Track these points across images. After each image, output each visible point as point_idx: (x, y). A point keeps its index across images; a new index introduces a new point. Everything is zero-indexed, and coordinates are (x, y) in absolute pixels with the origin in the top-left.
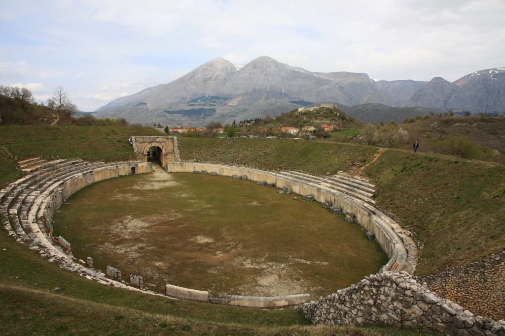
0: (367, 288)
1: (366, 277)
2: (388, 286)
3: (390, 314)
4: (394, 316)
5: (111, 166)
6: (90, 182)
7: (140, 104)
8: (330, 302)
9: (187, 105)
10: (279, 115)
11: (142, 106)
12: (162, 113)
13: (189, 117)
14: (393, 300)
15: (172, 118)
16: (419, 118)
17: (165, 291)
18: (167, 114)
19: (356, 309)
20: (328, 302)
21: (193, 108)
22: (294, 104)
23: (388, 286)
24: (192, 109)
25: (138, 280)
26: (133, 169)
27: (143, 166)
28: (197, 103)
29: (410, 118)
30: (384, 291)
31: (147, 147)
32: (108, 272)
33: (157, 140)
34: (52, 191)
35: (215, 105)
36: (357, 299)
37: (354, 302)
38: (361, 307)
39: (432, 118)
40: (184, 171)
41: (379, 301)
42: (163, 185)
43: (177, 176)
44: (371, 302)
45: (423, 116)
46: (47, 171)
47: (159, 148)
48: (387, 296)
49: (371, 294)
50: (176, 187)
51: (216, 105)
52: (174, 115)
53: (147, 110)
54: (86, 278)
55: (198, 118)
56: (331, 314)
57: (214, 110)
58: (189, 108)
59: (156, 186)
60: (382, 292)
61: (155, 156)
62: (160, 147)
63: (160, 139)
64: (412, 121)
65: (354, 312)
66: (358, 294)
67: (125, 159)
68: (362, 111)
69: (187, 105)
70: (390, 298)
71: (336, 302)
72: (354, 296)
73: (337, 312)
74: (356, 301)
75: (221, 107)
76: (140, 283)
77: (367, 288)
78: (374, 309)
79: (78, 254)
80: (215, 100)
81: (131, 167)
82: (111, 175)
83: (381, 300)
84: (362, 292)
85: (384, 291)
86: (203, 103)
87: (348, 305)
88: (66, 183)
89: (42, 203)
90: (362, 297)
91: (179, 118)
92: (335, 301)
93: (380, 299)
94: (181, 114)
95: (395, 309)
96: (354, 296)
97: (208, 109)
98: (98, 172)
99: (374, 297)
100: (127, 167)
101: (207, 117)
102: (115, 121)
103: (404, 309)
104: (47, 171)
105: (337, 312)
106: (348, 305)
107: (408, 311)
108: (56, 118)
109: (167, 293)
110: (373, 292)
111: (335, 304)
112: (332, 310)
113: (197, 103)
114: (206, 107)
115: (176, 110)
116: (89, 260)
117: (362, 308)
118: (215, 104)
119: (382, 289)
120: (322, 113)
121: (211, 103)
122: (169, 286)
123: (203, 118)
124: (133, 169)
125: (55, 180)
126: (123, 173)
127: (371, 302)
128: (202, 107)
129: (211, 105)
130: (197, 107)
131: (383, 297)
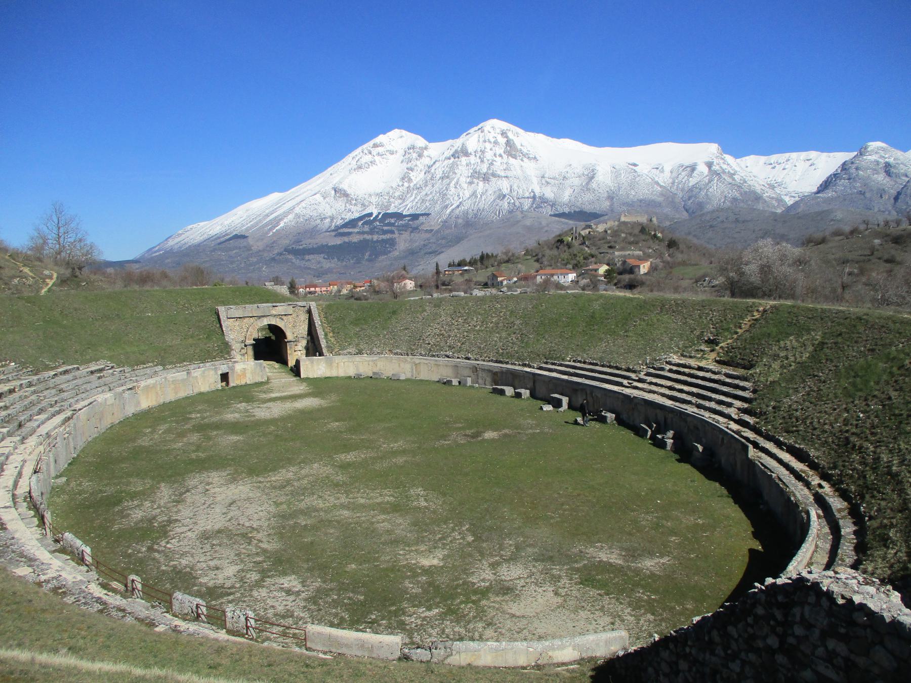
0: (760, 611)
1: (756, 584)
2: (809, 604)
3: (821, 669)
4: (831, 674)
5: (176, 375)
6: (130, 410)
7: (230, 239)
8: (676, 646)
9: (333, 234)
10: (531, 243)
11: (242, 243)
12: (281, 254)
13: (339, 260)
14: (824, 635)
15: (303, 263)
16: (837, 233)
17: (302, 641)
18: (290, 257)
19: (738, 662)
20: (671, 646)
21: (346, 239)
22: (563, 220)
23: (809, 604)
24: (345, 242)
25: (243, 619)
26: (225, 377)
27: (247, 369)
28: (356, 230)
29: (818, 235)
30: (802, 614)
31: (255, 330)
32: (176, 607)
33: (274, 312)
34: (48, 435)
35: (392, 232)
36: (740, 636)
37: (734, 646)
38: (750, 654)
39: (867, 232)
40: (334, 373)
41: (791, 640)
42: (289, 406)
43: (319, 386)
44: (773, 641)
45: (847, 229)
46: (34, 392)
47: (273, 329)
48: (809, 626)
49: (772, 623)
50: (320, 410)
51: (396, 232)
52: (307, 257)
53: (248, 248)
54: (484, 440)
55: (358, 262)
56: (681, 674)
57: (392, 243)
58: (338, 241)
59: (276, 410)
60: (798, 619)
61: (270, 347)
62: (280, 324)
63: (281, 308)
64: (823, 241)
65: (735, 666)
66: (740, 626)
67: (205, 357)
68: (711, 226)
69: (333, 234)
70: (817, 632)
71: (691, 647)
72: (731, 630)
73: (694, 669)
74: (736, 640)
75: (406, 235)
76: (248, 627)
77: (760, 611)
78: (780, 658)
79: (109, 570)
80: (393, 221)
81: (220, 372)
82: (176, 393)
83: (797, 637)
84: (750, 620)
85: (802, 614)
86: (366, 228)
87: (719, 651)
88: (78, 418)
89: (24, 461)
90: (750, 630)
91: (319, 263)
92: (689, 643)
93: (793, 635)
94: (322, 255)
95: (830, 657)
96: (731, 630)
97: (377, 241)
98: (147, 388)
99: (779, 630)
100: (212, 372)
101: (376, 257)
102: (709, 207)
103: (852, 657)
104: (34, 392)
105: (694, 669)
106: (719, 651)
107: (861, 661)
108: (51, 278)
109: (309, 645)
110: (776, 620)
111: (688, 650)
112: (683, 665)
113: (356, 230)
114: (375, 237)
115: (311, 246)
116: (133, 581)
117: (752, 657)
118: (393, 228)
119: (797, 611)
120: (623, 235)
121: (385, 228)
122: (314, 628)
123: (370, 260)
124: (225, 377)
125: (52, 410)
126: (204, 387)
127: (773, 641)
128: (368, 237)
129: (385, 232)
130: (355, 239)
131: (798, 631)
